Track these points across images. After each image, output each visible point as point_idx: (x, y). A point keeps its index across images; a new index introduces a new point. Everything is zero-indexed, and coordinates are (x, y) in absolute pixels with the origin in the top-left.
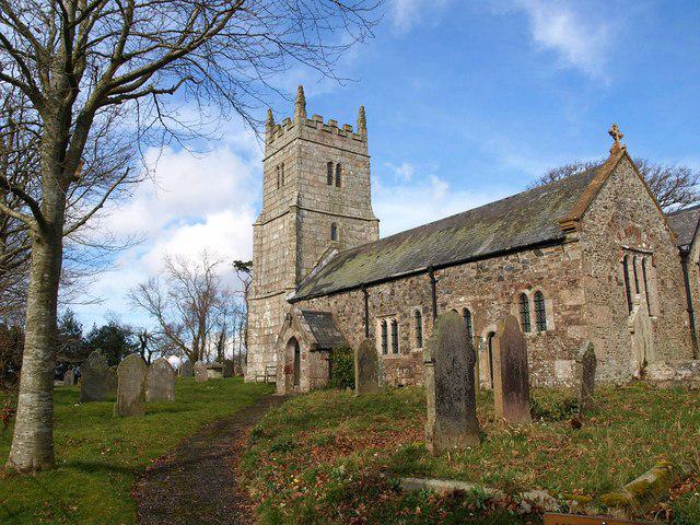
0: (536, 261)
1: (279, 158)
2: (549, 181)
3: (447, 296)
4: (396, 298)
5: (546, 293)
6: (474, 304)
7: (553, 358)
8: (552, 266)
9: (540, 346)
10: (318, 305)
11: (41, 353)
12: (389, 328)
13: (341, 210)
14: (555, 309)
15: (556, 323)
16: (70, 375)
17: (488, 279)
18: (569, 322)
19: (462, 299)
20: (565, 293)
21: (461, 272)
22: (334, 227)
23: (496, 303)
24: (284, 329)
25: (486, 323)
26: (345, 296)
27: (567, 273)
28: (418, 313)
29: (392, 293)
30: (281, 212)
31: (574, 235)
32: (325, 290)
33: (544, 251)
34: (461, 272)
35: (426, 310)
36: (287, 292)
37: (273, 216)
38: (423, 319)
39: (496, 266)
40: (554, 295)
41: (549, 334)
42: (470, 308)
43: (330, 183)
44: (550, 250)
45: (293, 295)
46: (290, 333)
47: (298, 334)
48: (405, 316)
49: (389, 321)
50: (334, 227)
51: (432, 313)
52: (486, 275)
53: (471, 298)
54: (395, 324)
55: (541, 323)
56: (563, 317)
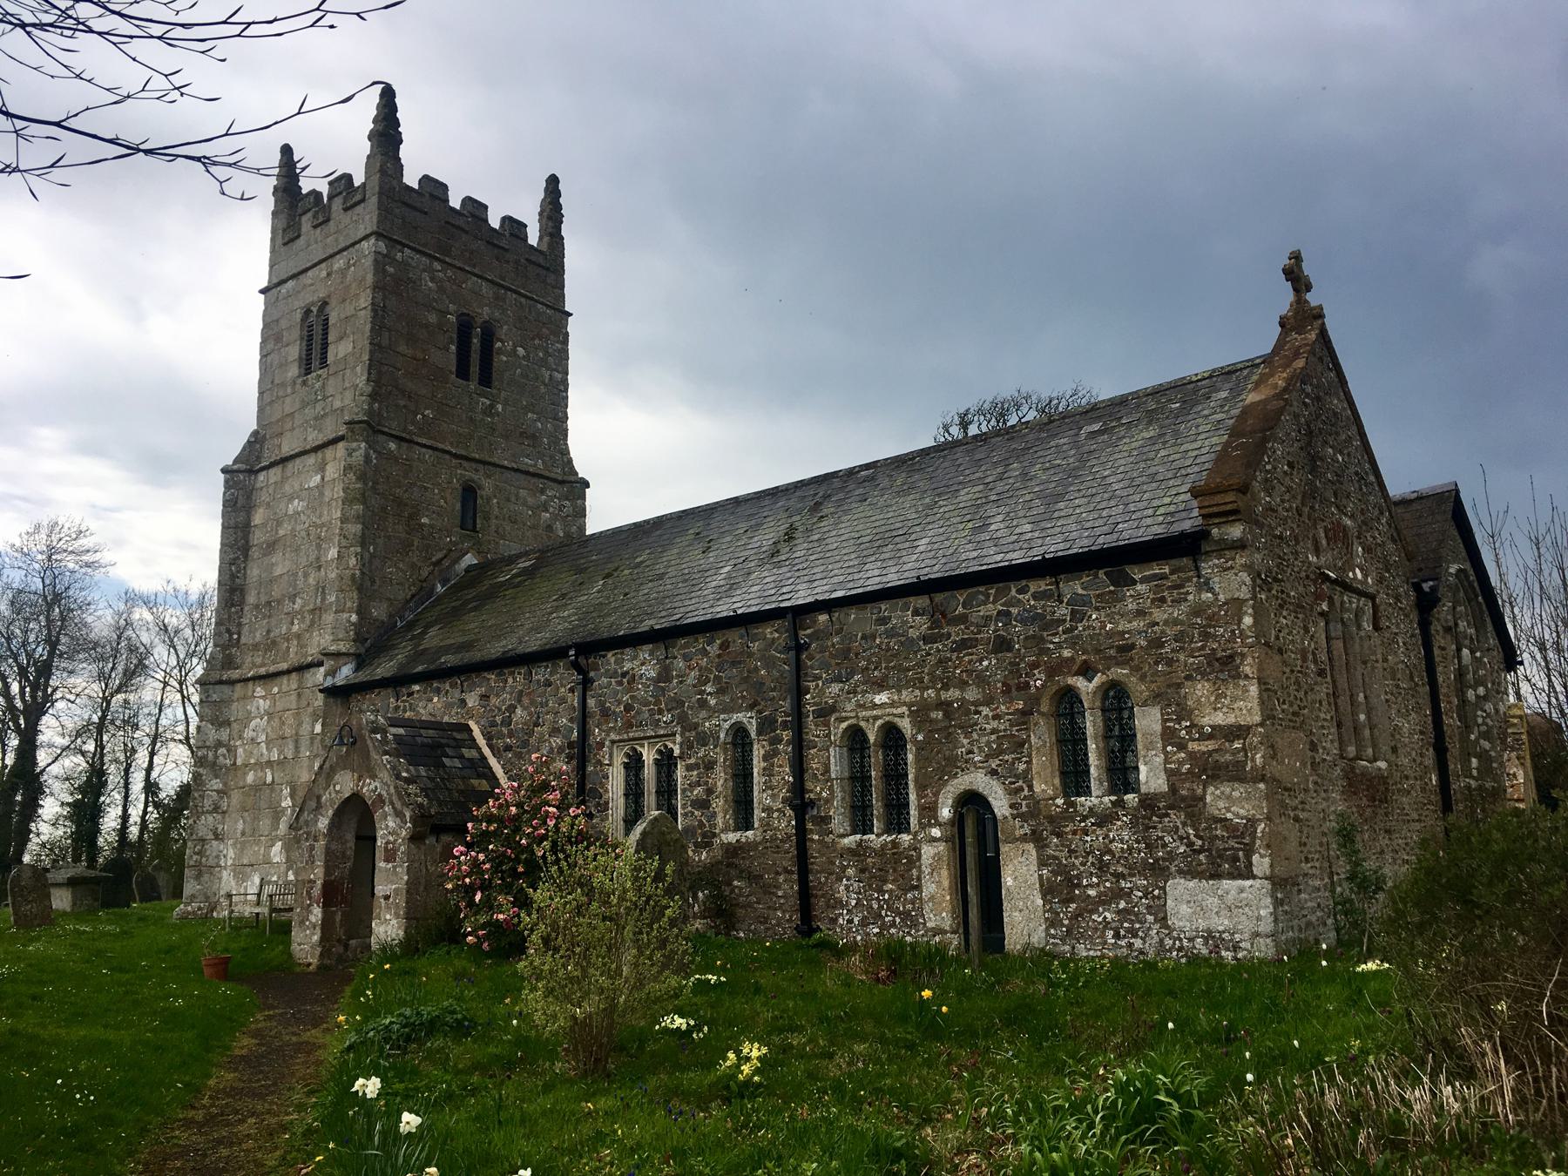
0: (1116, 598)
1: (313, 288)
2: (955, 431)
3: (835, 688)
4: (674, 688)
5: (1139, 689)
6: (920, 714)
8: (1159, 615)
9: (1121, 835)
10: (431, 705)
12: (649, 772)
13: (728, 659)
14: (1168, 736)
15: (1170, 774)
16: (296, 622)
17: (963, 645)
18: (1213, 771)
19: (882, 698)
20: (1201, 690)
22: (469, 493)
23: (985, 711)
24: (326, 774)
25: (952, 765)
26: (516, 680)
28: (739, 732)
29: (664, 675)
30: (314, 438)
31: (1236, 531)
32: (449, 660)
34: (883, 621)
35: (766, 726)
36: (329, 664)
37: (287, 450)
38: (758, 752)
39: (991, 609)
40: (1170, 698)
41: (1148, 802)
42: (906, 725)
43: (463, 372)
45: (346, 672)
46: (345, 784)
47: (370, 788)
48: (703, 740)
49: (649, 755)
50: (469, 493)
51: (786, 735)
52: (956, 633)
53: (906, 695)
54: (666, 763)
55: (1121, 776)
56: (1192, 756)
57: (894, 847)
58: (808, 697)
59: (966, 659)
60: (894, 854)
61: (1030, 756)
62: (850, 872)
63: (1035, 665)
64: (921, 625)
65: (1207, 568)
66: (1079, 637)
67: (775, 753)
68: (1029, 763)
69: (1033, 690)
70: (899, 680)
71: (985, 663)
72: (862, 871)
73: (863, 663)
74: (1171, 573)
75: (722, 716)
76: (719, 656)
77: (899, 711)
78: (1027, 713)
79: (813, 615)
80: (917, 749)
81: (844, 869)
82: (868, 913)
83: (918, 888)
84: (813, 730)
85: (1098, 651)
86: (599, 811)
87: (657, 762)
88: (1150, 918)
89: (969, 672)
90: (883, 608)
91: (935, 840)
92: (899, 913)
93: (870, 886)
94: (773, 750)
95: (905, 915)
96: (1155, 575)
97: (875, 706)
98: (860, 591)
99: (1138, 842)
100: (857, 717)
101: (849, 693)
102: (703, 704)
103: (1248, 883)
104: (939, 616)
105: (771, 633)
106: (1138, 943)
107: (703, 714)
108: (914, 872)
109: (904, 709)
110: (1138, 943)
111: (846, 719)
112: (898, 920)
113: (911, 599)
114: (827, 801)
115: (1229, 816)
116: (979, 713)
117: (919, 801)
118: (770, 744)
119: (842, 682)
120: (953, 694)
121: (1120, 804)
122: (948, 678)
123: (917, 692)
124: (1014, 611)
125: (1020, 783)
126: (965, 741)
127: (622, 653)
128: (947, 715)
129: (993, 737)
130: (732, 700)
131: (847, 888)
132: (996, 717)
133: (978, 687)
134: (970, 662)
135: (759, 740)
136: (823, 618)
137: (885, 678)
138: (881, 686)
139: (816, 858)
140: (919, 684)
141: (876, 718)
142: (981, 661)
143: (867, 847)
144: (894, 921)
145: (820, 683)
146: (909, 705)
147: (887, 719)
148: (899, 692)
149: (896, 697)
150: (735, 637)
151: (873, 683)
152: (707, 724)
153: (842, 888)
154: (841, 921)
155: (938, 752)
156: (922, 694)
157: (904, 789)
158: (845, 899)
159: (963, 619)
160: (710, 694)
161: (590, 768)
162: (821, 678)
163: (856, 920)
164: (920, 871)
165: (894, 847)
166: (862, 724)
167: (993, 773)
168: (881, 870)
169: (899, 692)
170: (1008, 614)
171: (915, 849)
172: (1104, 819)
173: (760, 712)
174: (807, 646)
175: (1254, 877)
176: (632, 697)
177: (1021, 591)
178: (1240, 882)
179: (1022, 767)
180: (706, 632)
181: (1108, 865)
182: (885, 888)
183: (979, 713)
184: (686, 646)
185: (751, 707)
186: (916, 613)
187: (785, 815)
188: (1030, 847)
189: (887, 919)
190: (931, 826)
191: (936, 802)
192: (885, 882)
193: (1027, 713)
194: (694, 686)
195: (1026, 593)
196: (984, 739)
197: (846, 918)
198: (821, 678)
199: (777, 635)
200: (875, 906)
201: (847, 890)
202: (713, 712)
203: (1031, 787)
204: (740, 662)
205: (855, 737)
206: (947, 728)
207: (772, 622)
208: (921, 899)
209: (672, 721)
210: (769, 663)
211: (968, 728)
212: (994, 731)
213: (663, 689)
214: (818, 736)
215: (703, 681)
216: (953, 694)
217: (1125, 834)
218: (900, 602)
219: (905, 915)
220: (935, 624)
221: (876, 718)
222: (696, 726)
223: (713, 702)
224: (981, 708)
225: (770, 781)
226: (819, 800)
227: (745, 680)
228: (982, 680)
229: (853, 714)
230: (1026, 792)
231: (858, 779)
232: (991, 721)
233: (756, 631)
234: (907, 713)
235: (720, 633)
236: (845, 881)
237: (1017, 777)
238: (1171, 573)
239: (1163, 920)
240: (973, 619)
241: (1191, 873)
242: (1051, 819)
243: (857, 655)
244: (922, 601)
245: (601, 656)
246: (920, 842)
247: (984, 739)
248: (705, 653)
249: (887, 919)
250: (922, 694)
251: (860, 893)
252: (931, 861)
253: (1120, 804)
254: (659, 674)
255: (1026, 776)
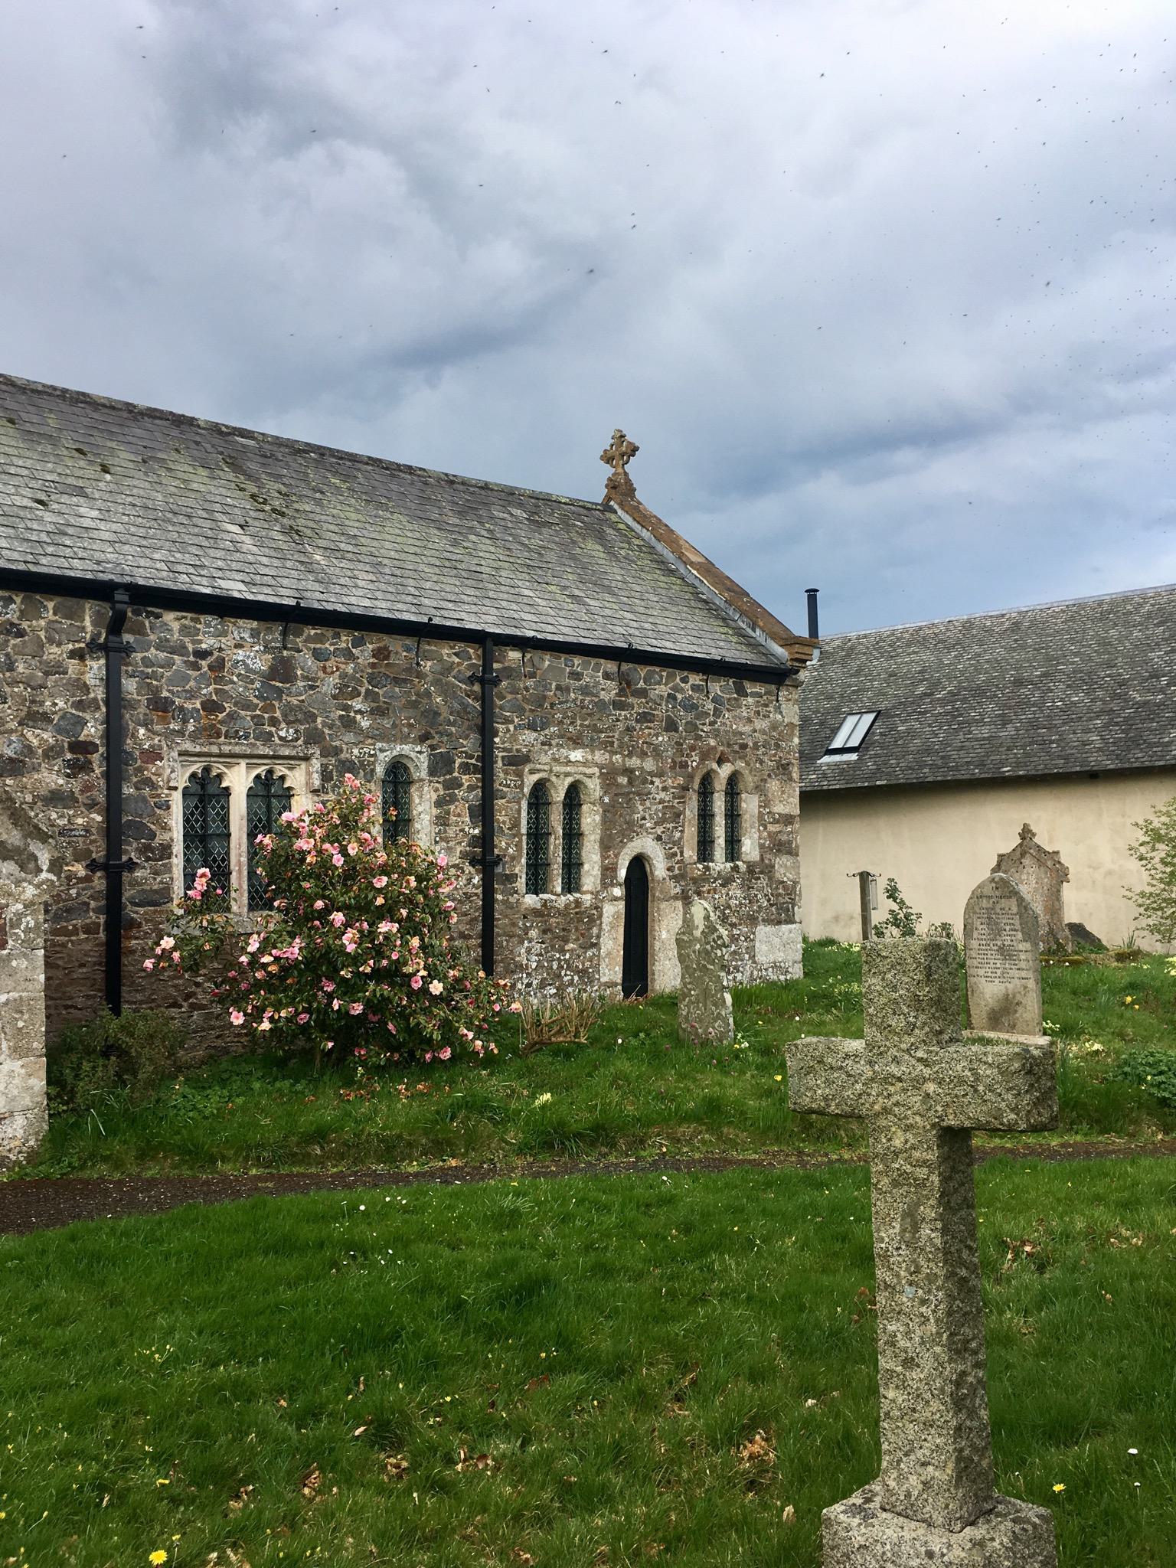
3: (529, 736)
4: (296, 695)
5: (749, 780)
6: (608, 777)
7: (752, 921)
11: (667, 991)
15: (762, 846)
17: (645, 718)
19: (577, 755)
21: (576, 676)
23: (657, 781)
25: (631, 829)
27: (778, 746)
29: (282, 671)
33: (750, 688)
44: (759, 689)
49: (239, 780)
52: (638, 705)
53: (600, 756)
56: (769, 833)
57: (576, 907)
58: (497, 740)
59: (646, 731)
60: (577, 913)
61: (683, 826)
62: (533, 933)
63: (693, 748)
64: (609, 691)
65: (783, 693)
66: (718, 730)
67: (453, 799)
68: (682, 832)
69: (690, 769)
70: (592, 739)
71: (660, 739)
72: (545, 932)
73: (559, 716)
74: (766, 694)
75: (379, 745)
76: (373, 666)
77: (588, 771)
78: (685, 788)
79: (503, 648)
80: (604, 811)
81: (526, 930)
82: (548, 974)
83: (596, 945)
84: (502, 776)
85: (729, 745)
86: (148, 859)
87: (251, 794)
88: (747, 956)
89: (649, 744)
90: (576, 663)
91: (616, 899)
92: (578, 972)
93: (553, 947)
94: (449, 795)
95: (583, 973)
96: (757, 693)
97: (569, 762)
98: (455, 624)
99: (745, 899)
100: (551, 771)
101: (543, 744)
102: (349, 723)
103: (794, 926)
104: (626, 683)
105: (449, 655)
106: (739, 976)
107: (350, 737)
108: (595, 931)
109: (596, 770)
110: (739, 976)
111: (539, 771)
112: (576, 978)
113: (602, 661)
114: (513, 858)
115: (785, 879)
116: (652, 783)
117: (602, 861)
118: (446, 788)
119: (536, 731)
120: (634, 762)
121: (736, 869)
122: (633, 746)
123: (607, 756)
124: (679, 696)
125: (676, 849)
126: (641, 808)
127: (197, 621)
128: (630, 782)
129: (661, 806)
130: (394, 726)
131: (529, 951)
132: (665, 789)
133: (654, 759)
134: (650, 734)
135: (431, 782)
136: (514, 655)
137: (580, 736)
138: (576, 742)
139: (499, 919)
140: (607, 745)
141: (567, 775)
142: (657, 735)
143: (552, 907)
144: (573, 980)
145: (511, 727)
146: (601, 767)
147: (578, 777)
148: (593, 752)
149: (590, 757)
150: (400, 648)
151: (569, 739)
152: (356, 751)
153: (523, 951)
154: (519, 986)
155: (621, 815)
156: (611, 758)
157: (544, 854)
158: (525, 962)
159: (643, 693)
160: (360, 712)
161: (128, 790)
162: (512, 722)
163: (535, 982)
164: (600, 929)
165: (576, 907)
166: (554, 779)
167: (659, 838)
168: (564, 930)
169: (593, 752)
170: (675, 698)
171: (596, 908)
172: (727, 881)
173: (432, 747)
174: (496, 682)
175: (795, 922)
176: (217, 691)
177: (685, 680)
178: (790, 926)
179: (678, 835)
180: (356, 630)
181: (727, 918)
182: (567, 948)
183: (652, 783)
184: (320, 639)
185: (423, 738)
186: (607, 676)
187: (463, 872)
188: (679, 904)
189: (565, 979)
190: (612, 885)
191: (617, 863)
192: (566, 941)
193: (685, 788)
194: (334, 697)
195: (687, 682)
196: (654, 808)
197: (525, 982)
198: (512, 722)
199: (457, 660)
200: (555, 967)
201: (528, 952)
202: (365, 735)
203: (682, 855)
204: (405, 681)
205: (539, 796)
206: (629, 793)
207: (452, 643)
208: (599, 956)
209: (297, 739)
210: (446, 690)
211: (644, 795)
212: (661, 801)
213: (280, 691)
214: (508, 786)
215: (346, 691)
216: (634, 762)
217: (739, 893)
218: (593, 661)
219: (583, 973)
220: (621, 692)
221: (567, 775)
222: (337, 751)
223: (365, 723)
224: (654, 779)
225: (445, 832)
226: (505, 856)
227: (414, 705)
228: (657, 754)
229: (546, 768)
230: (678, 858)
231: (538, 836)
232: (660, 792)
233: (427, 647)
234: (598, 774)
235: (375, 637)
236: (526, 944)
237: (674, 843)
238: (766, 694)
239: (752, 957)
240: (652, 694)
241: (768, 921)
242: (695, 880)
243: (552, 705)
244: (611, 666)
245: (149, 614)
246: (602, 901)
247: (654, 808)
248: (349, 656)
249: (565, 979)
250: (611, 758)
251: (541, 955)
252: (611, 919)
253: (736, 869)
254: (272, 668)
255: (678, 843)
